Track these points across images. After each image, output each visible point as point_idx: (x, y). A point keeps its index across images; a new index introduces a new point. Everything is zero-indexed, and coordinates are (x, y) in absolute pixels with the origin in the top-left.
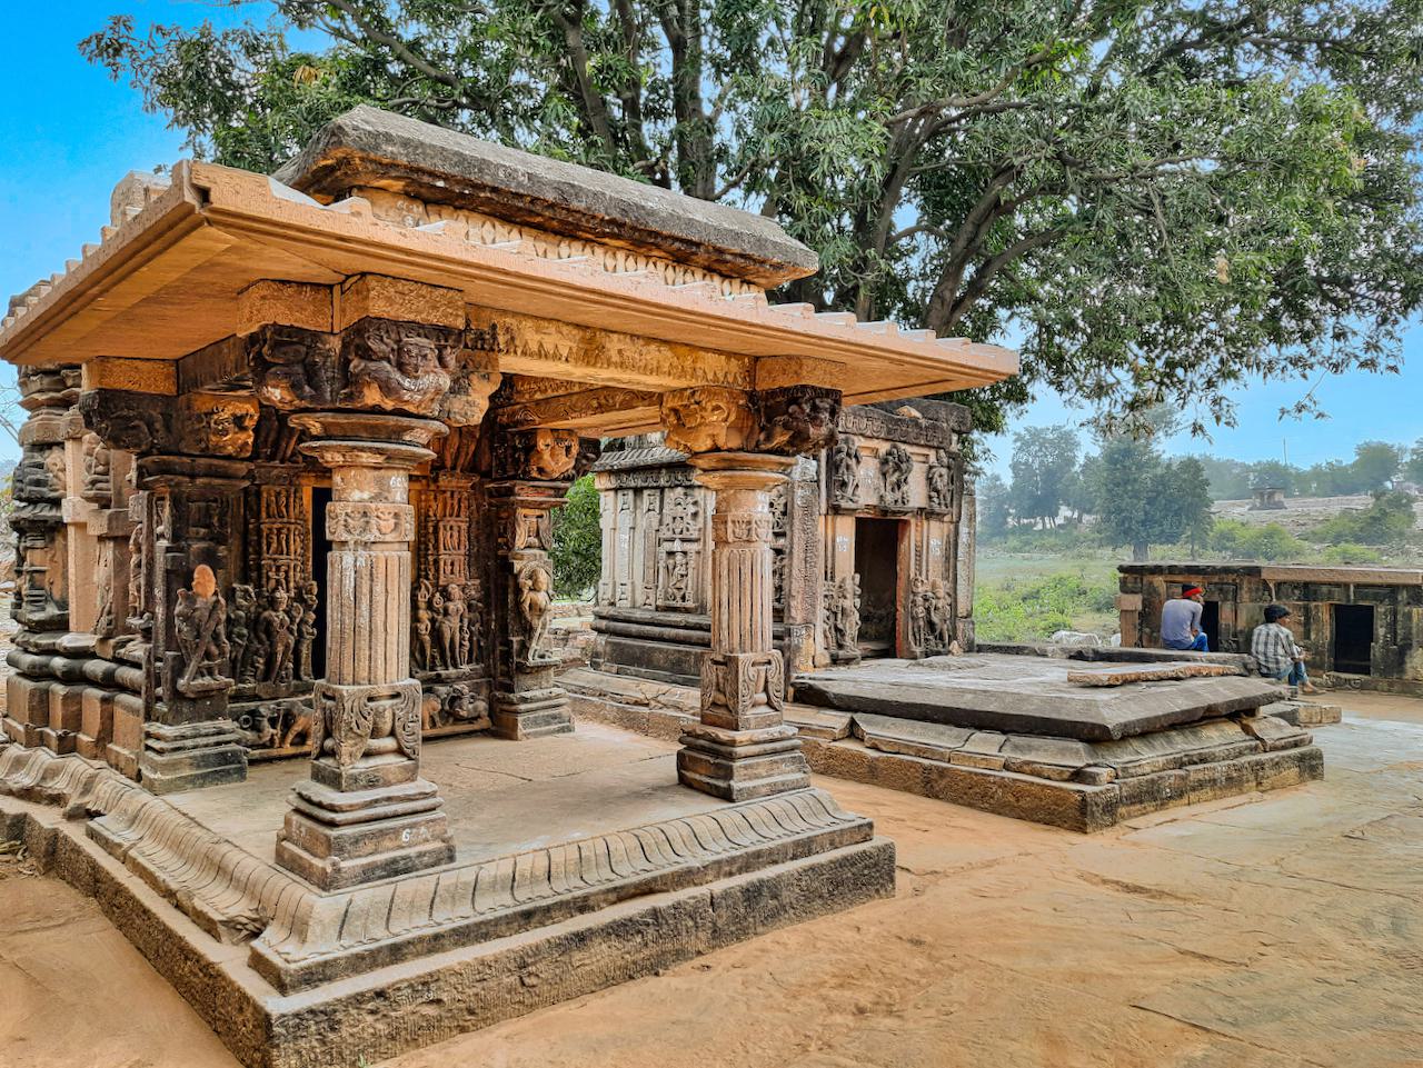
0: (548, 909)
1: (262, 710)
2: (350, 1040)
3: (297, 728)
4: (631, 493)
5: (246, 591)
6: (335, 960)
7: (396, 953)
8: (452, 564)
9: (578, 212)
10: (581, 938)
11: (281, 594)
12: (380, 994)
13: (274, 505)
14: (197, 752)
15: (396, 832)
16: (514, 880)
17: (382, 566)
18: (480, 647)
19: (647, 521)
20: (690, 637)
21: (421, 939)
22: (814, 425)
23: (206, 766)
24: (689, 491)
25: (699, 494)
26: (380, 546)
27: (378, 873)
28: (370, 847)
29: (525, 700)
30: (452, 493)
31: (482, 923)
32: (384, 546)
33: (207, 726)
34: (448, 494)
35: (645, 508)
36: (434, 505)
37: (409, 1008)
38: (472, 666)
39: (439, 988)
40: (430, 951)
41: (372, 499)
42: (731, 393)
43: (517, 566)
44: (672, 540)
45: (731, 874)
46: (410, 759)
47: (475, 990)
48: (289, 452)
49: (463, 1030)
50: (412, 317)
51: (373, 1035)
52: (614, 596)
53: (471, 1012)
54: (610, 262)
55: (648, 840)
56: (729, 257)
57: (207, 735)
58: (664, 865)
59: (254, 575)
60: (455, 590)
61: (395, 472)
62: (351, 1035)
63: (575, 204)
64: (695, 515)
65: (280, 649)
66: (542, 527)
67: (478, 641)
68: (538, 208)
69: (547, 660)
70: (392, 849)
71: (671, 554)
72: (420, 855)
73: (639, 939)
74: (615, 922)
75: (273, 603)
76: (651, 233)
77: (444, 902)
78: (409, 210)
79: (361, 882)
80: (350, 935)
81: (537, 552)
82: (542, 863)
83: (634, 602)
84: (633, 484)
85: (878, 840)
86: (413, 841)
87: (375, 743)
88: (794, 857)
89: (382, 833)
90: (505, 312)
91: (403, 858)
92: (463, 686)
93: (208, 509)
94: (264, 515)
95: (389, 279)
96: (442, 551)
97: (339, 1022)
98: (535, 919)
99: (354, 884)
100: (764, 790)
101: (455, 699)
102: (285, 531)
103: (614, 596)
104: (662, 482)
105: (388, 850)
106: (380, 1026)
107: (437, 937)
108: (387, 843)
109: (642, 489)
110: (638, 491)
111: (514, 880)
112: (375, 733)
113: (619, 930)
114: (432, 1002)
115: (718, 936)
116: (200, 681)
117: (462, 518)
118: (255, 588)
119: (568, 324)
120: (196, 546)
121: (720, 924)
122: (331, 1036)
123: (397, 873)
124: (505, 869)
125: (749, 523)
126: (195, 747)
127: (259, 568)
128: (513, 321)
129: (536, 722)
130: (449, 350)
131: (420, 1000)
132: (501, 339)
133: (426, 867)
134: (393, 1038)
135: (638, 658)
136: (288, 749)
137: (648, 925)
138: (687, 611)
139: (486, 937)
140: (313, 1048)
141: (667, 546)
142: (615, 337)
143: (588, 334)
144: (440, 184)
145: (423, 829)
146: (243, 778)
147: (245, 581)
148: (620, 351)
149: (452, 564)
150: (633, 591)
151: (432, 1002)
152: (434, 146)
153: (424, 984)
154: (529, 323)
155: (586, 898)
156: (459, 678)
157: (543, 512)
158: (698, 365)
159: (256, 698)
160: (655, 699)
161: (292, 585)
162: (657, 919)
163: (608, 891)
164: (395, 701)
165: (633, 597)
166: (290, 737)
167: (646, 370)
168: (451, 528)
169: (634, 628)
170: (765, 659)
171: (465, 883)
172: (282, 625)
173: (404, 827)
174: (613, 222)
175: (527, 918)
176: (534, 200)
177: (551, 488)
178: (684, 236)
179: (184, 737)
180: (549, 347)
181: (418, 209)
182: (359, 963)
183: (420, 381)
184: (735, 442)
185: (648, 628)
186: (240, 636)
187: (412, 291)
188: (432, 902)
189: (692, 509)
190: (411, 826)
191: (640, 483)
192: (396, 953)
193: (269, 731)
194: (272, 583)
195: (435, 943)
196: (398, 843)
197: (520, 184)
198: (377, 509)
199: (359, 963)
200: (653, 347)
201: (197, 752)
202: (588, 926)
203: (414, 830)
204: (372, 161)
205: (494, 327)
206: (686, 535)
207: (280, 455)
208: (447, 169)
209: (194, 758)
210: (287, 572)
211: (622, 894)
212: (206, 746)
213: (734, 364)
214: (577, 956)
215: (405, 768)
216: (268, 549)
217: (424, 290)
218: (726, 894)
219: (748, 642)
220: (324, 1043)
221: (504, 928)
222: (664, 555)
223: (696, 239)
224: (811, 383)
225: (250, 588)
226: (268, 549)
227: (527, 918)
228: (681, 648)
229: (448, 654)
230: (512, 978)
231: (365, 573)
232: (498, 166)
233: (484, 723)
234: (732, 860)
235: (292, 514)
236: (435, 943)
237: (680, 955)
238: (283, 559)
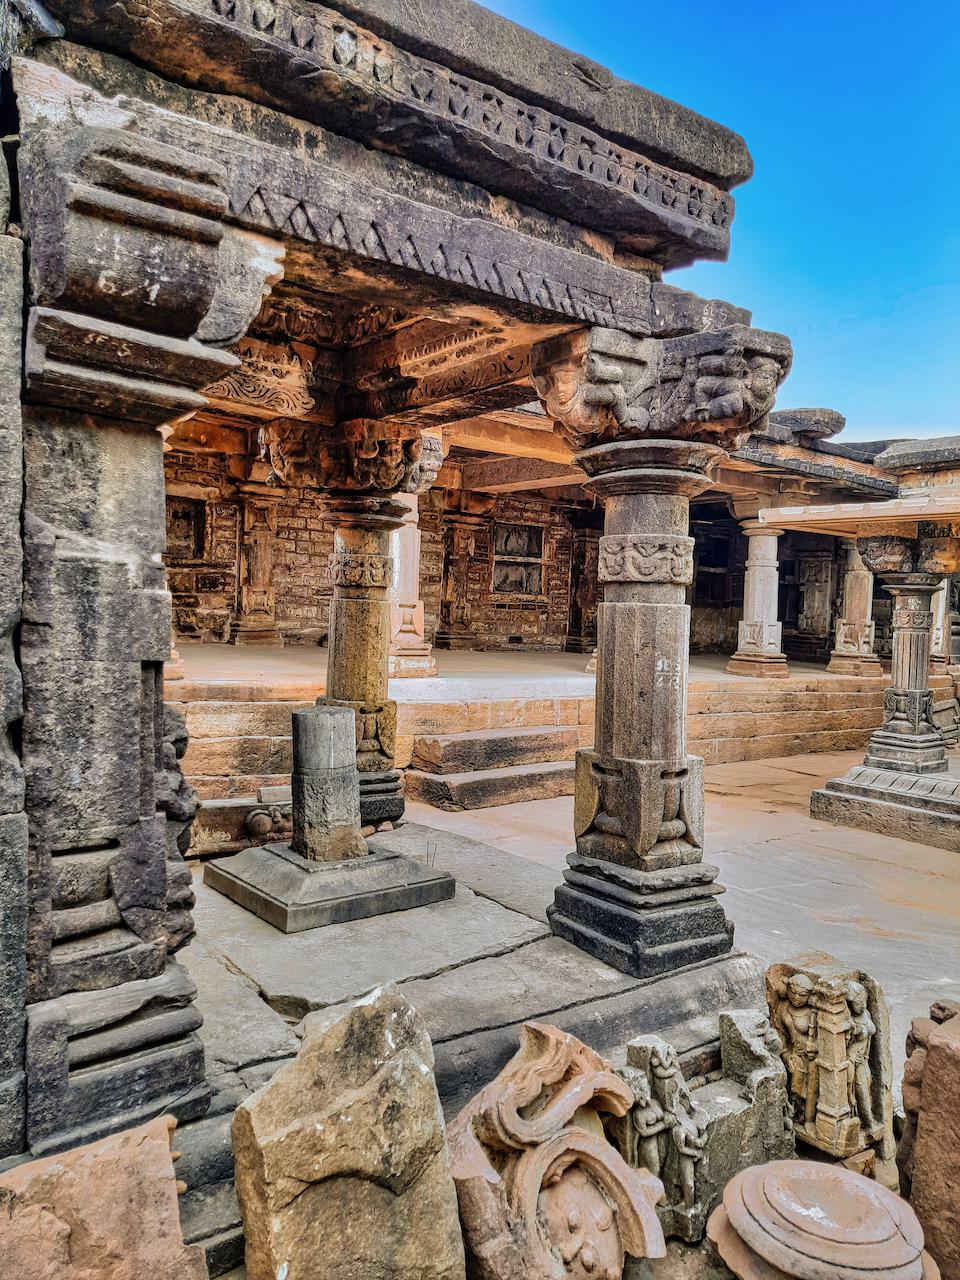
0: (937, 804)
10: (943, 821)
12: (847, 801)
15: (895, 752)
28: (883, 754)
87: (897, 714)
108: (890, 755)
112: (898, 710)
139: (905, 803)
175: (926, 803)
208: (918, 461)
214: (941, 829)
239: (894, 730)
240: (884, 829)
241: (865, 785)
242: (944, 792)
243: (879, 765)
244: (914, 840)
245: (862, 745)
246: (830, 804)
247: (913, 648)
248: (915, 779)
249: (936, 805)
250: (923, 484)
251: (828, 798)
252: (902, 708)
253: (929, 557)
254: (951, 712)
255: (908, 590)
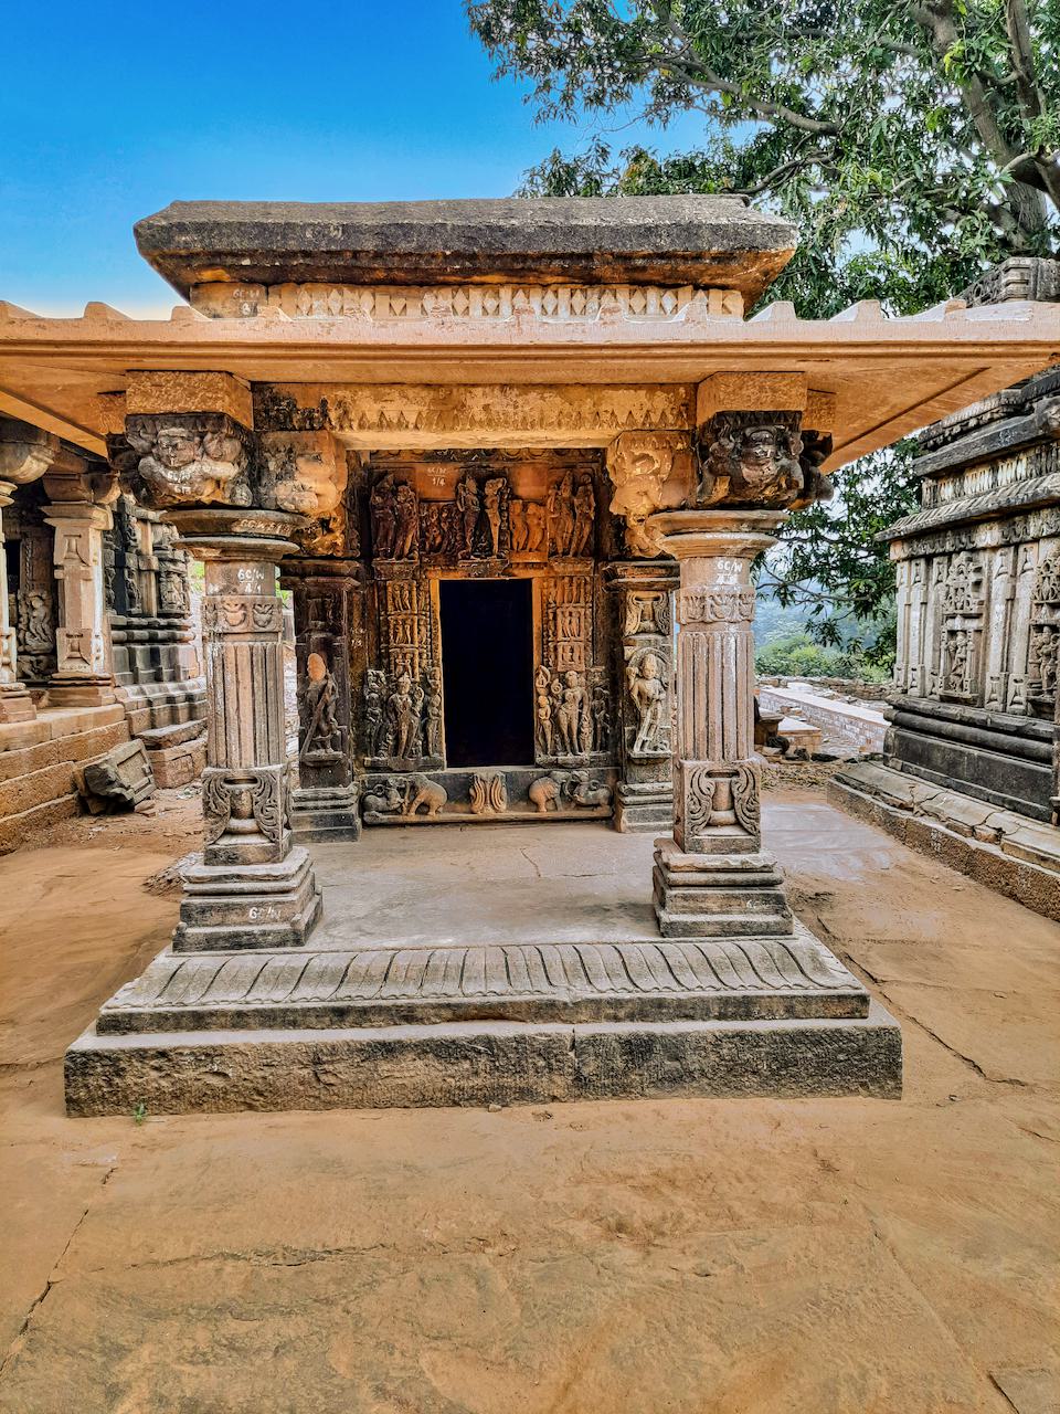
0: (364, 1011)
1: (390, 781)
2: (135, 1088)
3: (420, 799)
4: (922, 563)
5: (378, 676)
6: (140, 1014)
7: (199, 1020)
8: (572, 650)
9: (411, 254)
10: (389, 1049)
11: (406, 680)
12: (163, 1054)
13: (398, 599)
14: (317, 813)
15: (243, 908)
16: (345, 975)
17: (231, 656)
18: (606, 735)
19: (937, 593)
20: (964, 734)
21: (224, 1014)
22: (749, 465)
23: (325, 825)
24: (974, 556)
25: (983, 558)
26: (230, 637)
27: (221, 943)
28: (217, 918)
29: (633, 792)
30: (571, 578)
31: (288, 1010)
32: (235, 637)
33: (329, 791)
34: (566, 580)
35: (934, 581)
36: (554, 593)
37: (192, 1074)
38: (593, 754)
39: (222, 1063)
40: (234, 1026)
41: (222, 592)
42: (660, 438)
43: (628, 651)
44: (953, 617)
45: (616, 1019)
46: (750, 834)
47: (262, 1073)
48: (407, 550)
49: (251, 1107)
50: (169, 408)
51: (158, 1089)
52: (906, 682)
53: (260, 1094)
54: (490, 303)
55: (518, 960)
56: (639, 262)
57: (325, 799)
58: (525, 991)
59: (385, 661)
60: (572, 677)
61: (243, 564)
62: (136, 1084)
63: (403, 246)
64: (978, 584)
65: (405, 728)
66: (657, 610)
67: (604, 729)
68: (364, 262)
69: (659, 752)
70: (240, 924)
71: (953, 633)
72: (264, 934)
73: (466, 1065)
74: (432, 1040)
75: (397, 688)
76: (515, 257)
77: (266, 982)
78: (246, 297)
79: (204, 949)
80: (171, 995)
81: (652, 637)
82: (456, 960)
83: (923, 689)
84: (922, 552)
85: (878, 1017)
86: (259, 919)
87: (235, 823)
88: (721, 1017)
89: (228, 908)
90: (336, 385)
91: (247, 934)
92: (583, 774)
93: (324, 602)
94: (390, 608)
95: (146, 374)
96: (560, 637)
97: (123, 1069)
98: (350, 1019)
99: (198, 949)
100: (710, 929)
101: (575, 785)
102: (409, 622)
103: (906, 682)
104: (948, 547)
105: (235, 924)
106: (163, 1083)
107: (240, 1014)
108: (233, 917)
109: (935, 555)
110: (929, 559)
111: (345, 975)
112: (235, 813)
113: (446, 1051)
114: (217, 1074)
115: (582, 1085)
116: (314, 753)
117: (582, 603)
118: (386, 672)
119: (414, 385)
120: (316, 636)
121: (586, 1071)
122: (117, 1080)
123: (240, 946)
124: (339, 962)
125: (703, 599)
126: (316, 808)
127: (388, 655)
128: (348, 393)
129: (643, 817)
130: (209, 436)
131: (204, 1070)
132: (333, 415)
133: (272, 945)
134: (177, 1097)
135: (921, 756)
136: (413, 817)
137: (479, 1052)
138: (966, 702)
139: (294, 1024)
140: (101, 1087)
141: (951, 625)
142: (478, 391)
143: (442, 393)
144: (246, 262)
145: (270, 910)
146: (354, 838)
147: (378, 668)
148: (486, 408)
149: (572, 650)
150: (923, 676)
151: (217, 1074)
152: (231, 224)
153: (207, 1055)
154: (367, 392)
155: (411, 1008)
156: (580, 765)
157: (659, 594)
158: (603, 408)
159: (390, 770)
160: (918, 804)
161: (417, 670)
162: (491, 1049)
163: (440, 1006)
164: (251, 786)
165: (923, 684)
166: (414, 807)
167: (526, 424)
168: (571, 614)
169: (918, 720)
170: (729, 769)
171: (293, 969)
172: (405, 707)
173: (251, 905)
174: (457, 255)
175: (340, 1015)
176: (355, 254)
177: (660, 567)
178: (561, 250)
179: (306, 799)
180: (391, 413)
181: (256, 293)
182: (162, 1022)
183: (182, 472)
184: (674, 498)
185: (930, 721)
186: (374, 715)
187: (168, 381)
188: (255, 981)
189: (973, 577)
190: (258, 905)
191: (930, 551)
192: (199, 1020)
193: (396, 798)
194: (400, 669)
195: (239, 1020)
196: (244, 919)
197: (332, 240)
198: (223, 602)
199: (162, 1022)
200: (533, 395)
201: (317, 813)
202: (397, 1038)
203: (261, 910)
204: (172, 256)
205: (324, 403)
206: (967, 610)
207: (397, 552)
208: (246, 245)
209: (315, 817)
210: (412, 659)
211: (460, 1012)
212: (325, 808)
213: (661, 401)
214: (384, 1067)
215: (265, 849)
216: (395, 638)
217: (182, 378)
218: (594, 1041)
219: (703, 748)
220: (111, 1085)
221: (313, 1020)
222: (946, 635)
223: (579, 250)
224: (736, 407)
225: (381, 673)
226: (395, 638)
227: (340, 1015)
228: (958, 747)
229: (567, 739)
230: (305, 1072)
231: (219, 662)
232: (304, 227)
233: (604, 811)
234: (618, 1003)
235: (415, 605)
236: (239, 1020)
237: (526, 1094)
238: (408, 648)
239: (232, 859)
240: (261, 1097)
241: (193, 1002)
242: (367, 978)
243: (210, 944)
244: (329, 1105)
245: (23, 840)
246: (119, 1073)
247: (258, 678)
248: (343, 992)
249: (363, 1016)
250: (247, 308)
251: (113, 1061)
252: (245, 808)
253: (285, 474)
254: (138, 759)
255: (243, 549)
